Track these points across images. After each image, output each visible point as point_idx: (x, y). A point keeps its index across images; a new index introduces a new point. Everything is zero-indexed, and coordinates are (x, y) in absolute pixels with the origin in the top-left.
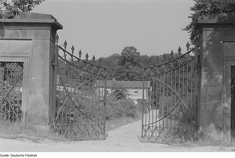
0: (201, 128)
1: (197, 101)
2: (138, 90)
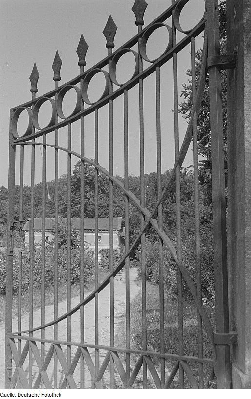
2: (101, 233)
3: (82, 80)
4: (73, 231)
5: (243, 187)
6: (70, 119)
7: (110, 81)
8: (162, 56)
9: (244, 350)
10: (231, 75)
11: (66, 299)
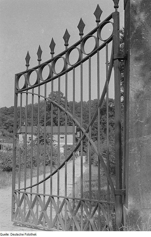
0: (130, 201)
1: (120, 135)
3: (52, 61)
4: (47, 134)
5: (129, 119)
6: (46, 81)
7: (66, 63)
8: (92, 52)
9: (128, 197)
10: (125, 63)
11: (43, 174)
